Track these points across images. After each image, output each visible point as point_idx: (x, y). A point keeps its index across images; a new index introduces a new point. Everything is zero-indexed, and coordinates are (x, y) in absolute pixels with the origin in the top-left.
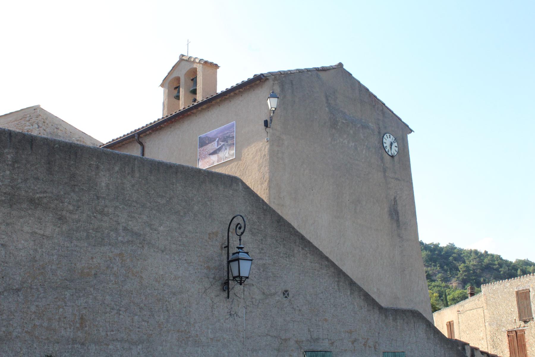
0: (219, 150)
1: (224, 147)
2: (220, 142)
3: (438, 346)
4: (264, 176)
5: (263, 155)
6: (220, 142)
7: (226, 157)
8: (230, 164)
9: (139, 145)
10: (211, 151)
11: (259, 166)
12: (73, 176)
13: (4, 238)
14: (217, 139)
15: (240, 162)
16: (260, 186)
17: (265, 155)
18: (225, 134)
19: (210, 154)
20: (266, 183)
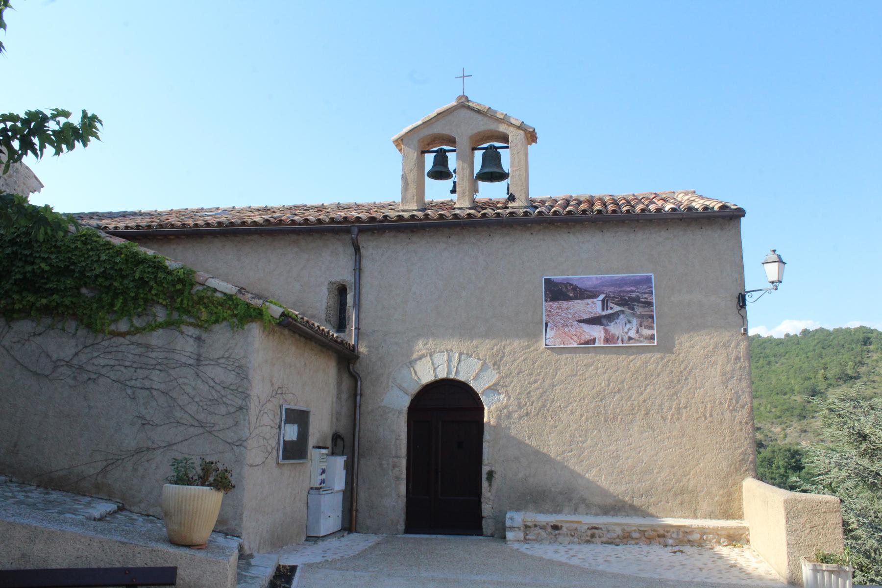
0: (611, 318)
1: (622, 316)
2: (610, 305)
3: (370, 408)
4: (738, 397)
5: (733, 357)
6: (610, 305)
7: (630, 338)
8: (645, 352)
9: (352, 250)
10: (585, 317)
11: (724, 374)
12: (218, 547)
13: (148, 267)
14: (602, 297)
15: (668, 356)
16: (727, 415)
17: (738, 358)
18: (624, 291)
19: (580, 321)
20: (744, 411)
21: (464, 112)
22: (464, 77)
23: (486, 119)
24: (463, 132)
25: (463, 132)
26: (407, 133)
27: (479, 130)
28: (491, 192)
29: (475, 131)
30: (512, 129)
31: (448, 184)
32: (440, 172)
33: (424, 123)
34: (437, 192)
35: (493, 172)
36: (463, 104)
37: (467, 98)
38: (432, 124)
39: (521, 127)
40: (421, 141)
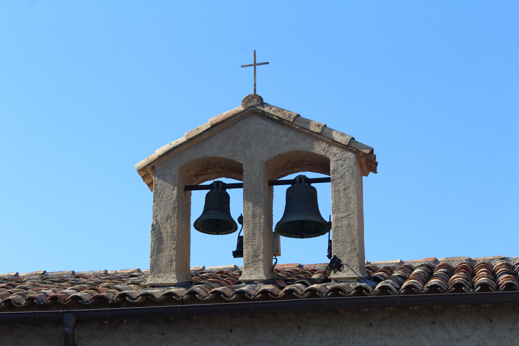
21: (256, 123)
22: (255, 65)
26: (160, 157)
27: (281, 152)
29: (276, 153)
31: (230, 241)
33: (189, 140)
36: (255, 109)
39: (351, 146)
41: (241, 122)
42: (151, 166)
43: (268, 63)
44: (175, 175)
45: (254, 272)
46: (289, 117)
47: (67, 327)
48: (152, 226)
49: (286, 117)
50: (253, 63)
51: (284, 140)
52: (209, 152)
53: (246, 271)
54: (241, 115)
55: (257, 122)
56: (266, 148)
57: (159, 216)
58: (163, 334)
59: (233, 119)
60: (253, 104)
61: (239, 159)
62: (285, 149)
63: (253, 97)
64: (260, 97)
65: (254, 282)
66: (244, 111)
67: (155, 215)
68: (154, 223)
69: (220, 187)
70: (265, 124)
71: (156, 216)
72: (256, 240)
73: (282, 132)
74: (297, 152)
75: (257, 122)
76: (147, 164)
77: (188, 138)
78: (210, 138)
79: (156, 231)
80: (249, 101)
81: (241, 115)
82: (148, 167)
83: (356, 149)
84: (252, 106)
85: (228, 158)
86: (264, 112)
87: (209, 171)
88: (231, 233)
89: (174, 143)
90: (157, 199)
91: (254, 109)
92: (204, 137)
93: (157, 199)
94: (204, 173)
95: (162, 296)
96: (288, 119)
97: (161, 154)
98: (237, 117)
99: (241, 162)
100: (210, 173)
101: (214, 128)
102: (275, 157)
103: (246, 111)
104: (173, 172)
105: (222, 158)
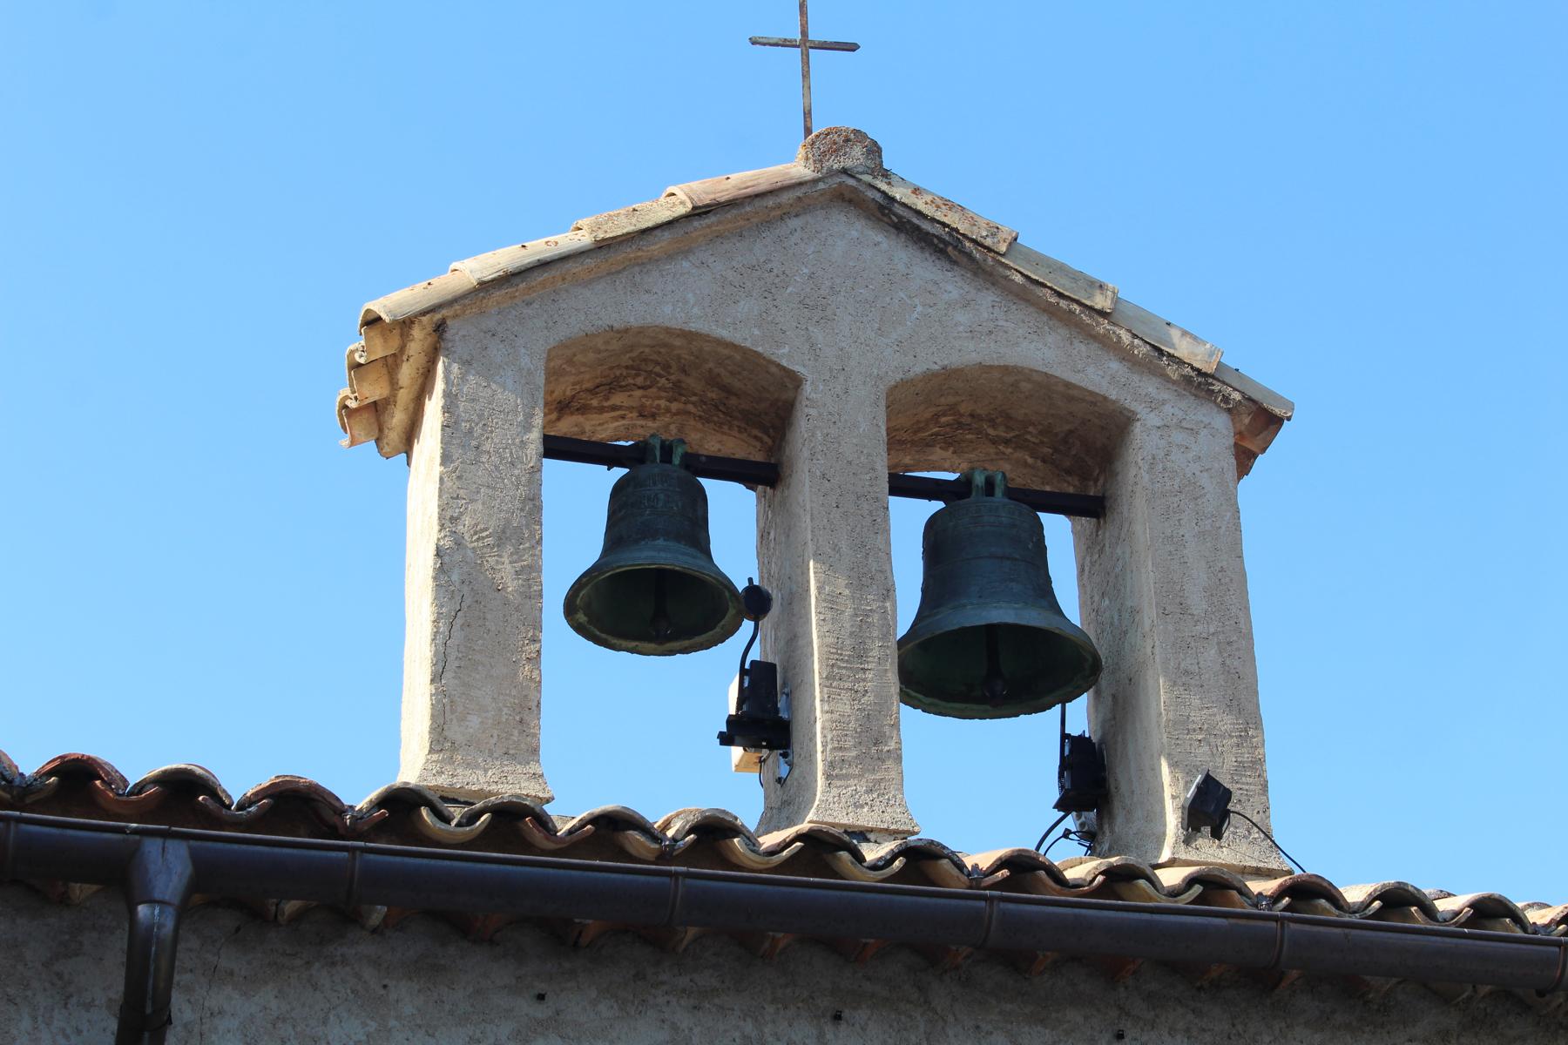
21: (852, 241)
22: (806, 45)
23: (987, 299)
24: (855, 341)
25: (855, 341)
26: (485, 287)
27: (955, 360)
28: (978, 791)
29: (927, 361)
30: (1150, 386)
31: (711, 678)
32: (649, 599)
33: (603, 246)
34: (635, 743)
35: (977, 661)
36: (854, 187)
37: (874, 150)
38: (768, 223)
39: (1202, 384)
40: (559, 363)
41: (794, 223)
42: (438, 316)
43: (852, 47)
44: (530, 372)
45: (868, 798)
46: (993, 235)
47: (151, 901)
48: (439, 553)
49: (979, 233)
50: (814, 35)
51: (963, 317)
52: (668, 309)
53: (835, 791)
54: (799, 193)
55: (855, 234)
56: (894, 336)
57: (467, 520)
58: (541, 997)
59: (770, 202)
60: (849, 163)
61: (787, 355)
62: (968, 352)
63: (847, 140)
64: (875, 143)
65: (872, 836)
66: (815, 181)
67: (449, 514)
68: (447, 543)
69: (676, 460)
70: (884, 246)
71: (453, 520)
72: (870, 675)
73: (950, 288)
74: (1006, 370)
75: (855, 234)
76: (425, 305)
77: (601, 236)
78: (670, 257)
79: (455, 577)
80: (835, 150)
81: (799, 193)
82: (425, 319)
83: (1242, 393)
84: (845, 171)
85: (748, 344)
86: (893, 199)
87: (618, 399)
88: (685, 651)
89: (539, 247)
90: (456, 452)
91: (851, 182)
92: (657, 245)
93: (456, 452)
94: (595, 403)
95: (583, 823)
96: (988, 242)
97: (488, 275)
98: (786, 198)
99: (796, 368)
100: (614, 408)
101: (696, 224)
102: (929, 376)
103: (821, 186)
104: (525, 361)
105: (720, 342)
